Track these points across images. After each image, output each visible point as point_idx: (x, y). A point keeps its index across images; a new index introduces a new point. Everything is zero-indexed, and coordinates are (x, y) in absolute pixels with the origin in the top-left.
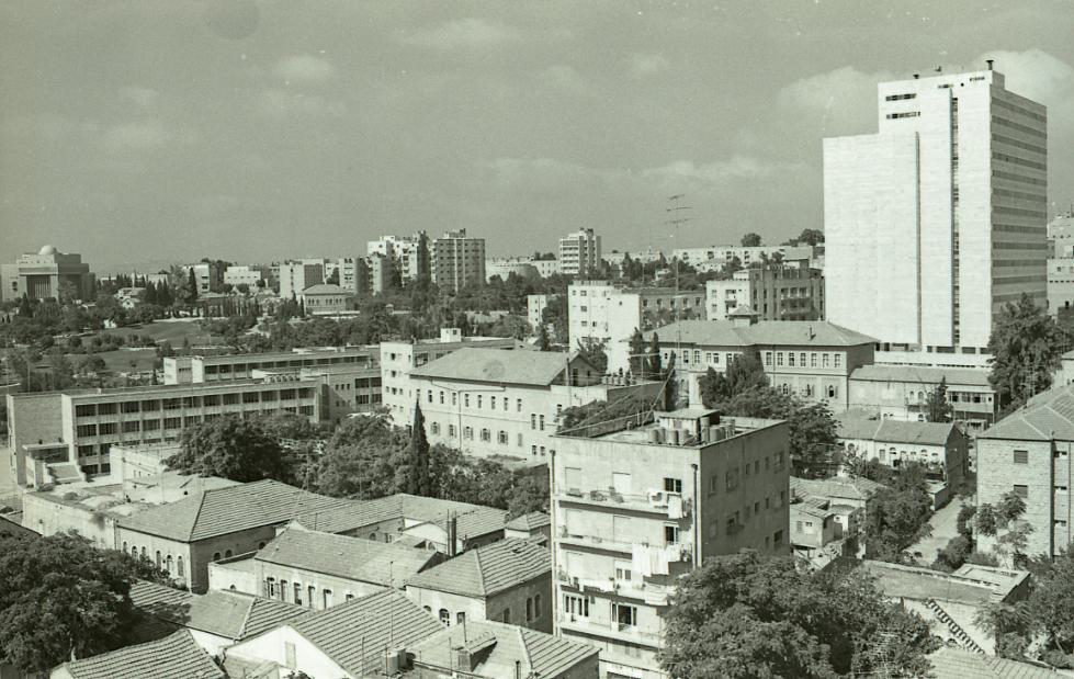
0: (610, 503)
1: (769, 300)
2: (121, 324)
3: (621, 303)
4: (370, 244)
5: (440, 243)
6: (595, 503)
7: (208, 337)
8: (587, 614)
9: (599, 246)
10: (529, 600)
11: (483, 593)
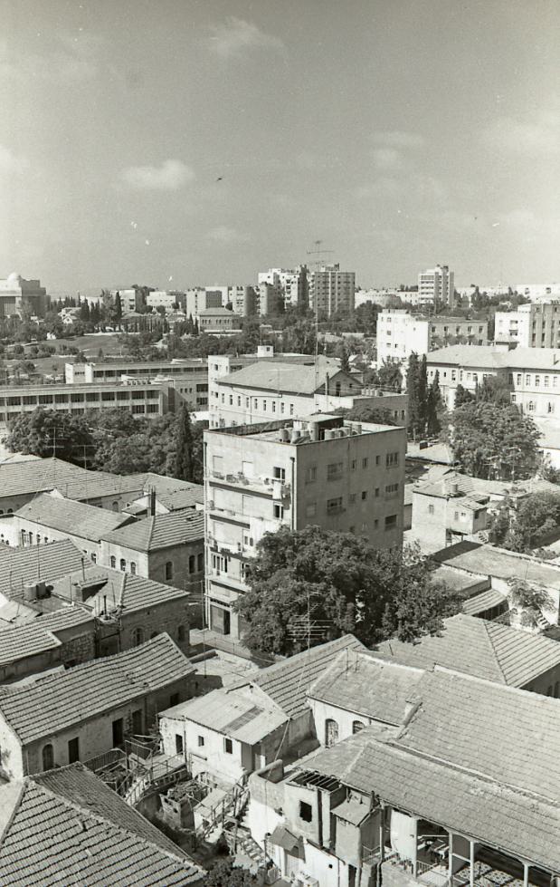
0: (240, 485)
1: (547, 330)
2: (60, 337)
3: (415, 329)
4: (260, 275)
5: (318, 275)
6: (229, 484)
7: (121, 348)
8: (226, 571)
9: (452, 280)
10: (192, 558)
11: (146, 549)
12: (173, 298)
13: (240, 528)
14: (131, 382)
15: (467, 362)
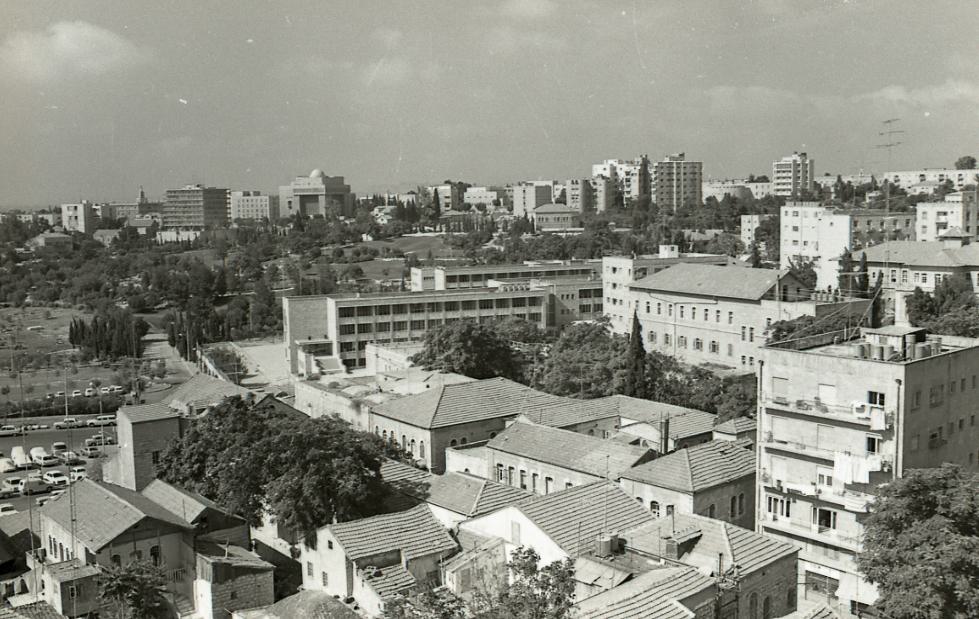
0: (814, 412)
2: (377, 238)
4: (595, 167)
5: (661, 166)
7: (449, 249)
8: (788, 515)
13: (812, 465)
15: (915, 261)
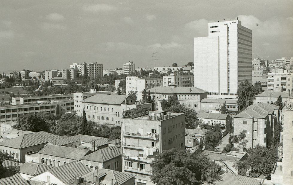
0: (137, 136)
1: (180, 81)
3: (140, 82)
4: (70, 65)
5: (90, 65)
8: (131, 166)
9: (134, 66)
12: (39, 74)
14: (44, 103)
